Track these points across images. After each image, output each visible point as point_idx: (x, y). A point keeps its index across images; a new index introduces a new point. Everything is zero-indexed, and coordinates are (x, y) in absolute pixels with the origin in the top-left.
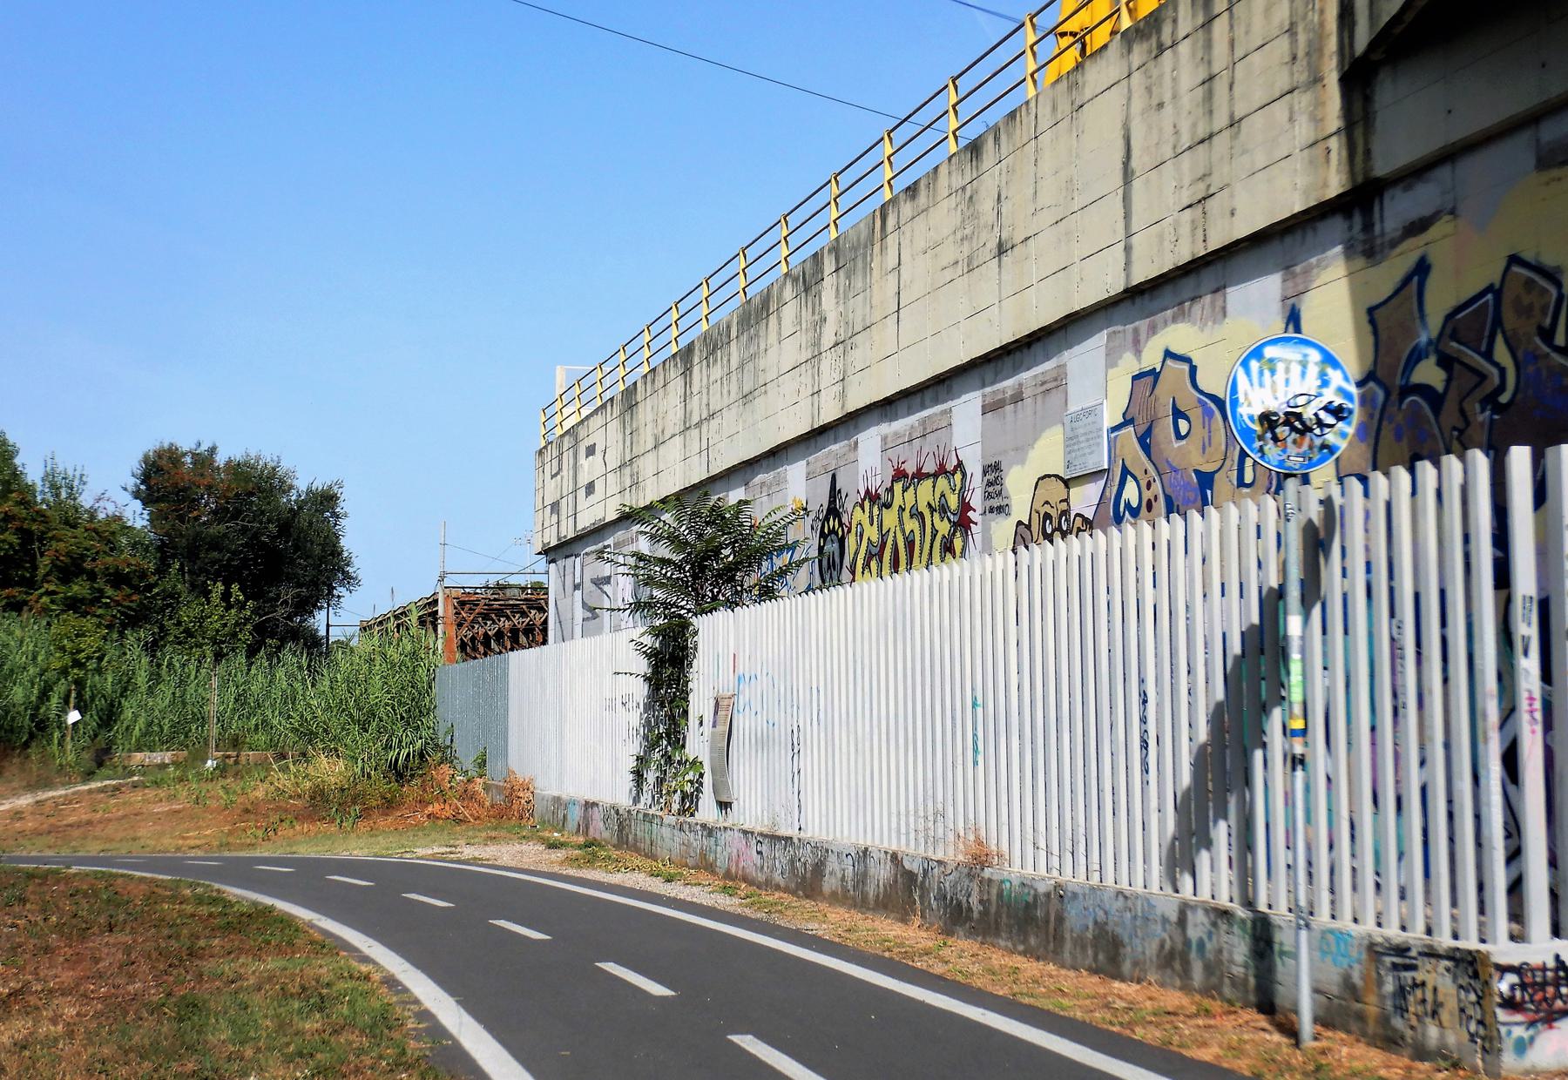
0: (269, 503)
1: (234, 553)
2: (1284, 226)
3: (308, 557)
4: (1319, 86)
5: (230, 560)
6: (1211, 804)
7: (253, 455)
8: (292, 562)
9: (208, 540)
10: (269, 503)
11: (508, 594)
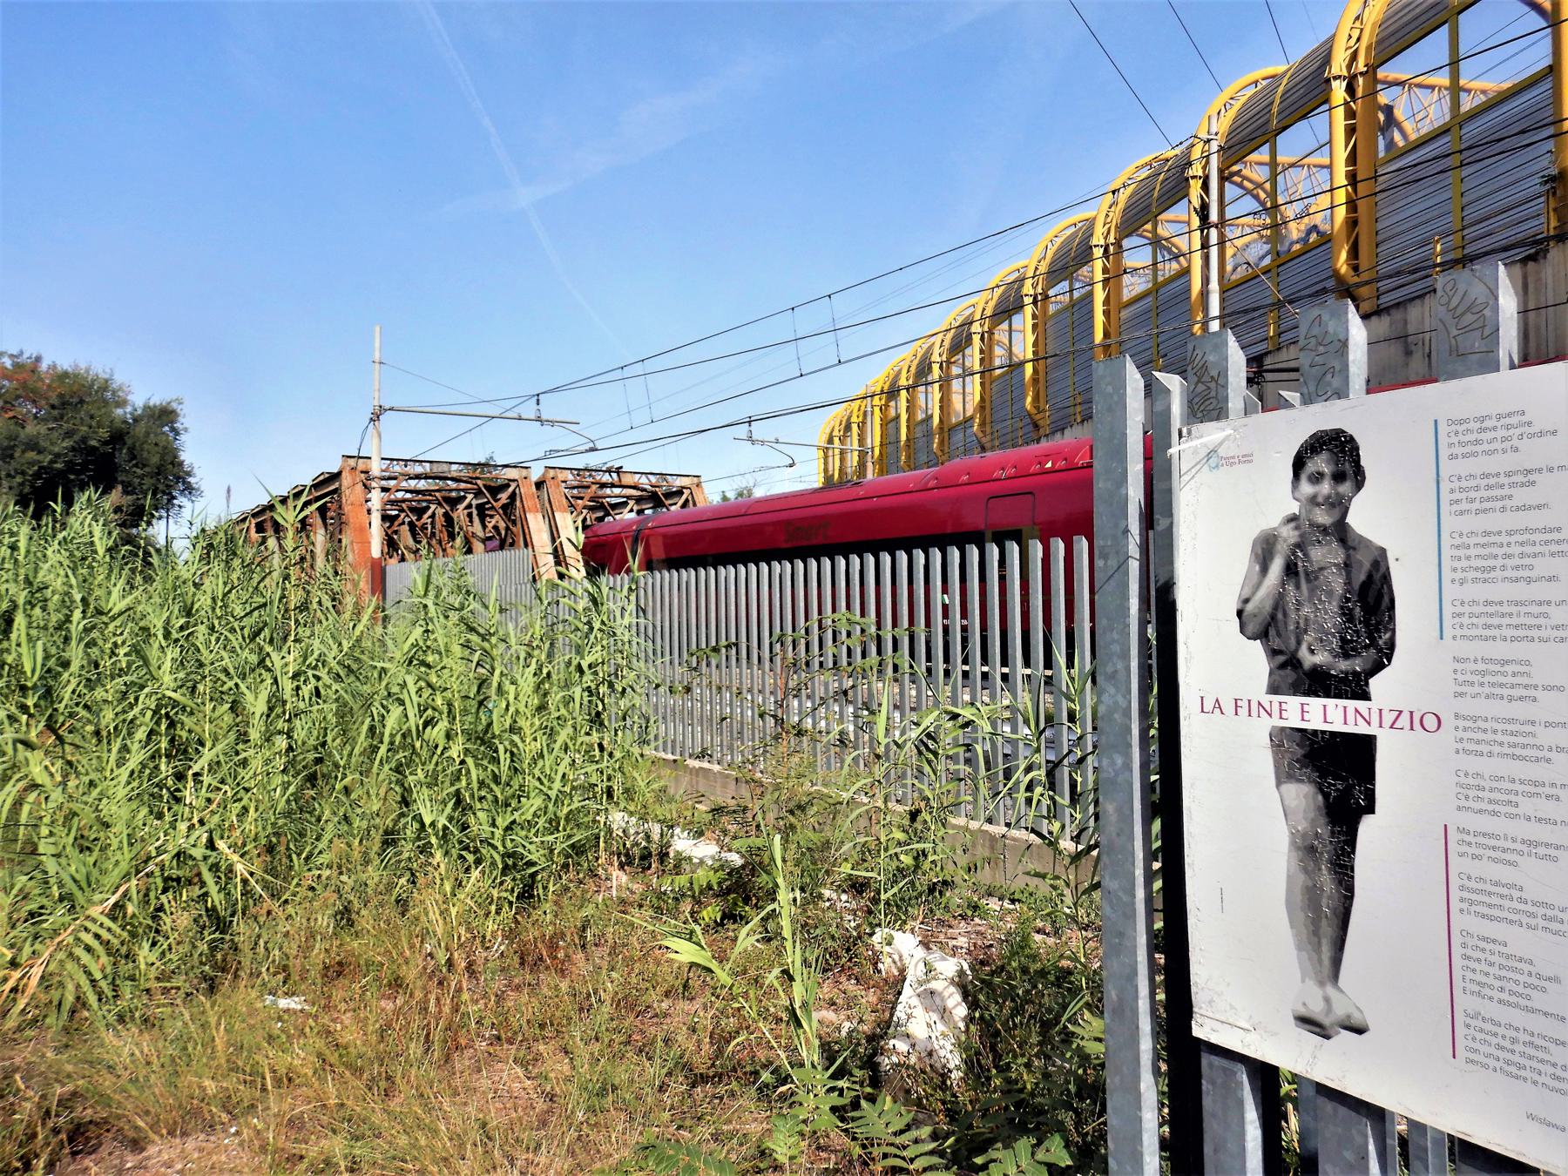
1: (57, 455)
3: (144, 466)
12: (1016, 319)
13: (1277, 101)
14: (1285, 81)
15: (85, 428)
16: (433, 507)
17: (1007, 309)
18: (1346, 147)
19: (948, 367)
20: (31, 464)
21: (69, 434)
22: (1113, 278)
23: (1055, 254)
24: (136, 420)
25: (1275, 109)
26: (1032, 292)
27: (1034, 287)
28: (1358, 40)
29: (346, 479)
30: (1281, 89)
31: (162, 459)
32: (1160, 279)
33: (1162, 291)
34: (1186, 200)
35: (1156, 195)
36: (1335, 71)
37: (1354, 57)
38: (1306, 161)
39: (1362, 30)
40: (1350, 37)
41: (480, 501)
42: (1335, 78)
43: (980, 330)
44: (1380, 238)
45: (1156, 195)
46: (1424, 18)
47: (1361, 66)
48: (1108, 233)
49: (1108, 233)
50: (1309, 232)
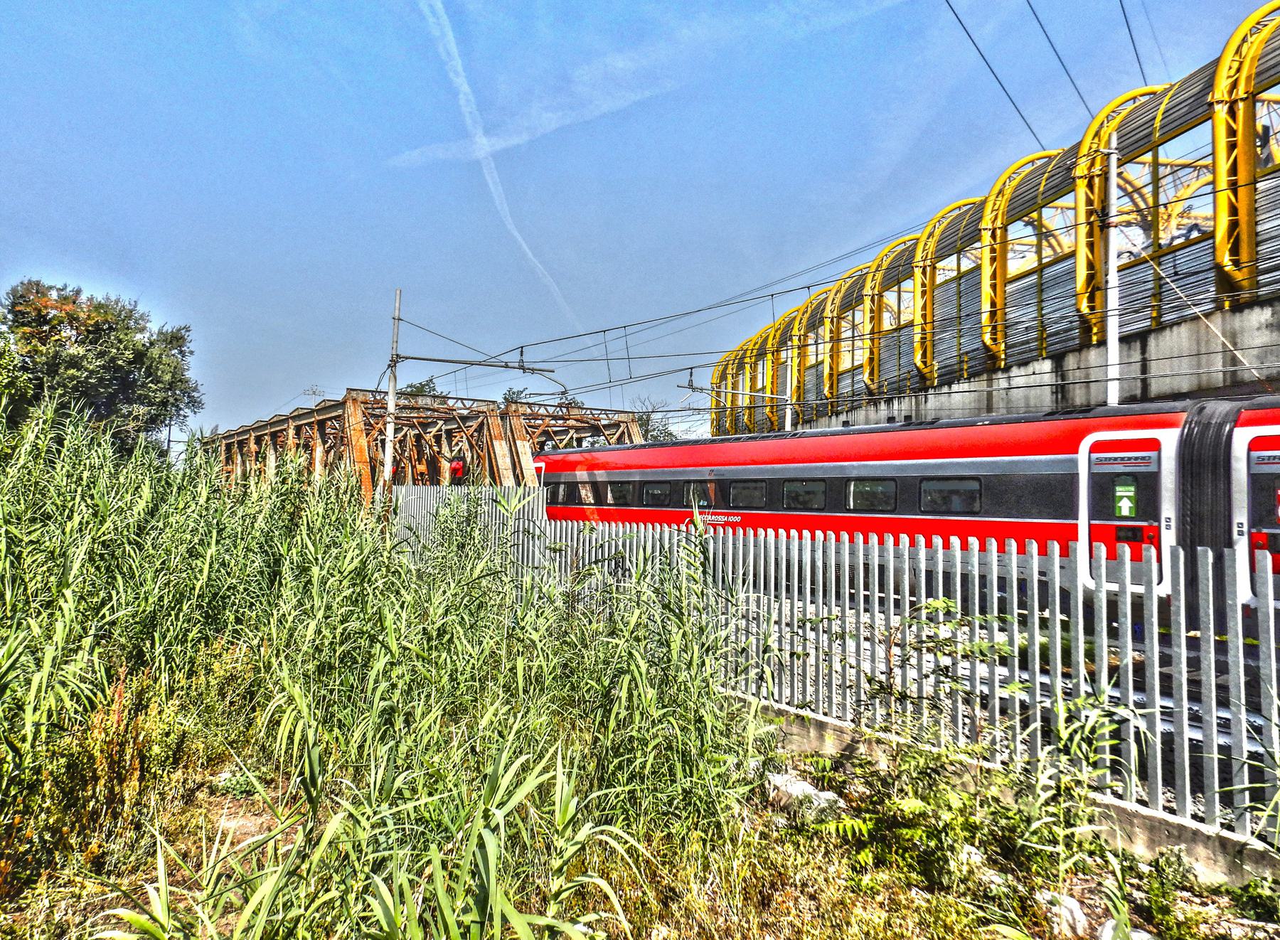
0: (126, 334)
1: (92, 372)
2: (1189, 564)
3: (158, 382)
4: (1102, 348)
5: (87, 378)
6: (1265, 531)
7: (113, 298)
8: (144, 385)
9: (68, 359)
10: (126, 334)
11: (420, 402)
12: (907, 285)
13: (1159, 117)
14: (1166, 100)
15: (115, 351)
16: (406, 429)
17: (897, 273)
18: (1228, 158)
19: (838, 323)
20: (72, 378)
21: (101, 355)
22: (999, 257)
23: (943, 233)
24: (152, 344)
25: (1157, 124)
26: (870, 293)
27: (873, 289)
28: (1238, 70)
29: (350, 408)
30: (1163, 107)
31: (173, 377)
32: (902, 323)
33: (1046, 271)
34: (1210, 122)
35: (1041, 189)
36: (1218, 96)
37: (1234, 85)
38: (1200, 163)
39: (1241, 63)
40: (1230, 68)
41: (449, 427)
42: (1218, 102)
43: (870, 293)
44: (1260, 238)
45: (1041, 189)
46: (1017, 210)
47: (1241, 92)
48: (996, 218)
49: (996, 218)
50: (1190, 230)
